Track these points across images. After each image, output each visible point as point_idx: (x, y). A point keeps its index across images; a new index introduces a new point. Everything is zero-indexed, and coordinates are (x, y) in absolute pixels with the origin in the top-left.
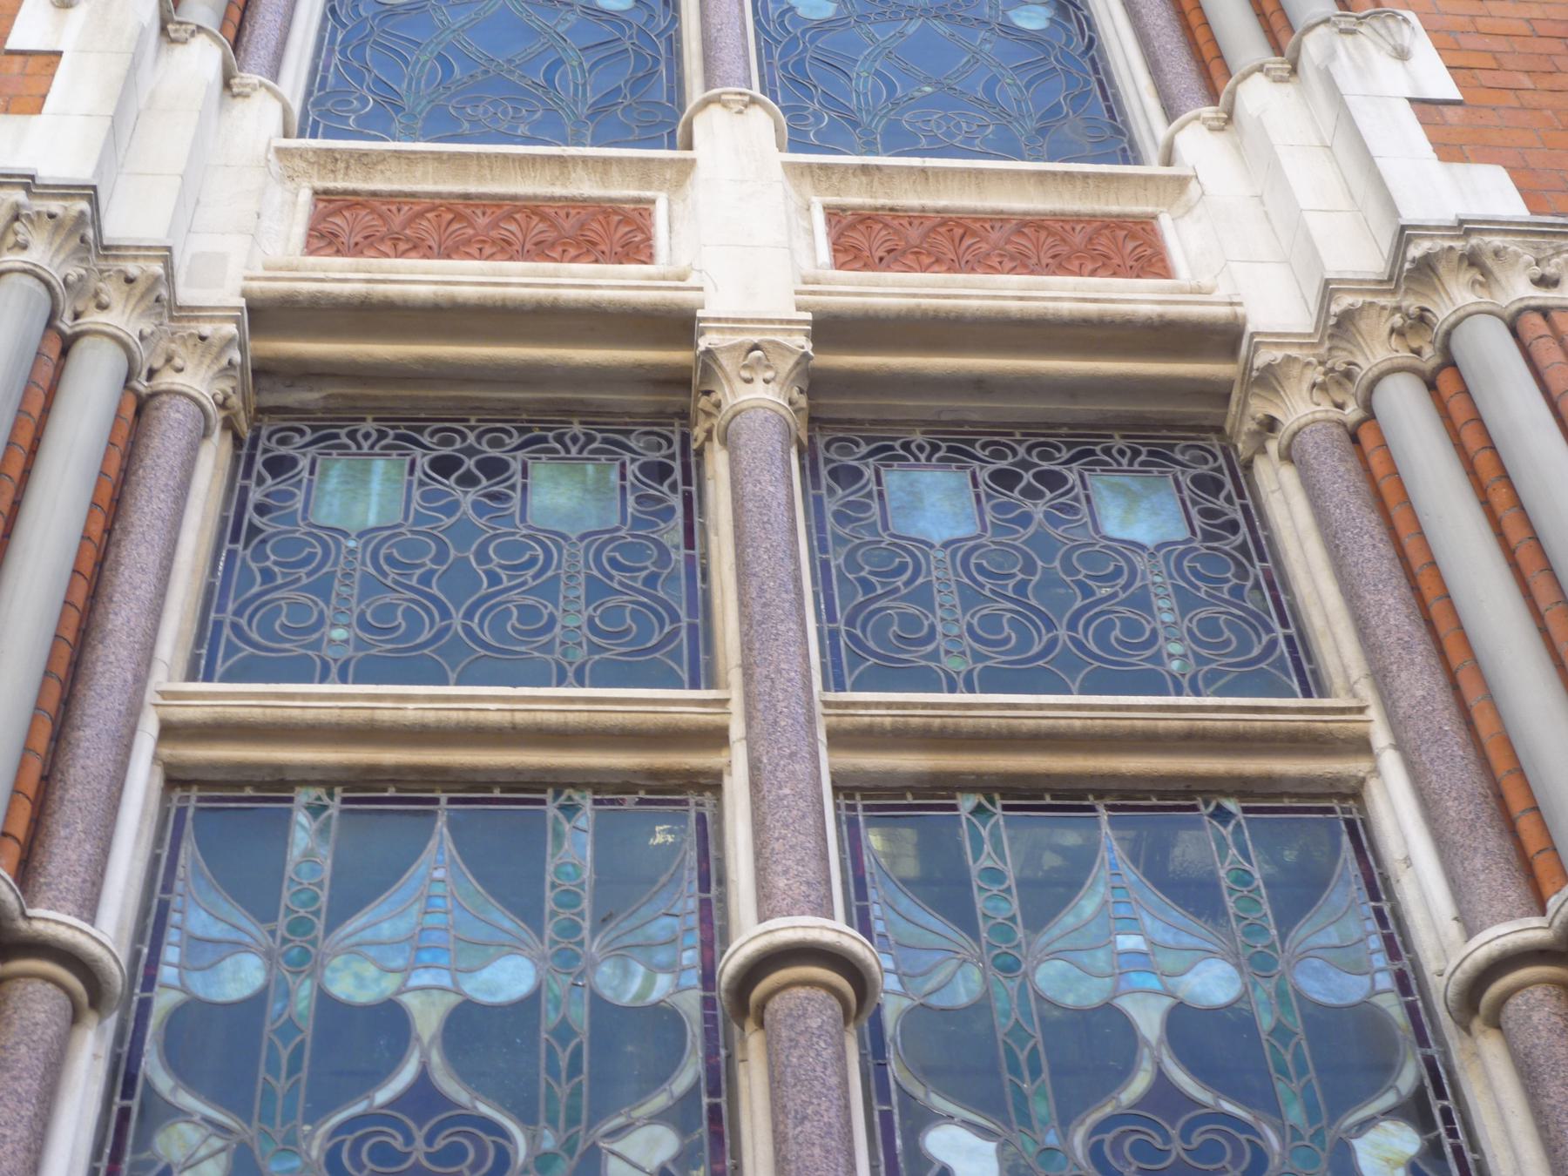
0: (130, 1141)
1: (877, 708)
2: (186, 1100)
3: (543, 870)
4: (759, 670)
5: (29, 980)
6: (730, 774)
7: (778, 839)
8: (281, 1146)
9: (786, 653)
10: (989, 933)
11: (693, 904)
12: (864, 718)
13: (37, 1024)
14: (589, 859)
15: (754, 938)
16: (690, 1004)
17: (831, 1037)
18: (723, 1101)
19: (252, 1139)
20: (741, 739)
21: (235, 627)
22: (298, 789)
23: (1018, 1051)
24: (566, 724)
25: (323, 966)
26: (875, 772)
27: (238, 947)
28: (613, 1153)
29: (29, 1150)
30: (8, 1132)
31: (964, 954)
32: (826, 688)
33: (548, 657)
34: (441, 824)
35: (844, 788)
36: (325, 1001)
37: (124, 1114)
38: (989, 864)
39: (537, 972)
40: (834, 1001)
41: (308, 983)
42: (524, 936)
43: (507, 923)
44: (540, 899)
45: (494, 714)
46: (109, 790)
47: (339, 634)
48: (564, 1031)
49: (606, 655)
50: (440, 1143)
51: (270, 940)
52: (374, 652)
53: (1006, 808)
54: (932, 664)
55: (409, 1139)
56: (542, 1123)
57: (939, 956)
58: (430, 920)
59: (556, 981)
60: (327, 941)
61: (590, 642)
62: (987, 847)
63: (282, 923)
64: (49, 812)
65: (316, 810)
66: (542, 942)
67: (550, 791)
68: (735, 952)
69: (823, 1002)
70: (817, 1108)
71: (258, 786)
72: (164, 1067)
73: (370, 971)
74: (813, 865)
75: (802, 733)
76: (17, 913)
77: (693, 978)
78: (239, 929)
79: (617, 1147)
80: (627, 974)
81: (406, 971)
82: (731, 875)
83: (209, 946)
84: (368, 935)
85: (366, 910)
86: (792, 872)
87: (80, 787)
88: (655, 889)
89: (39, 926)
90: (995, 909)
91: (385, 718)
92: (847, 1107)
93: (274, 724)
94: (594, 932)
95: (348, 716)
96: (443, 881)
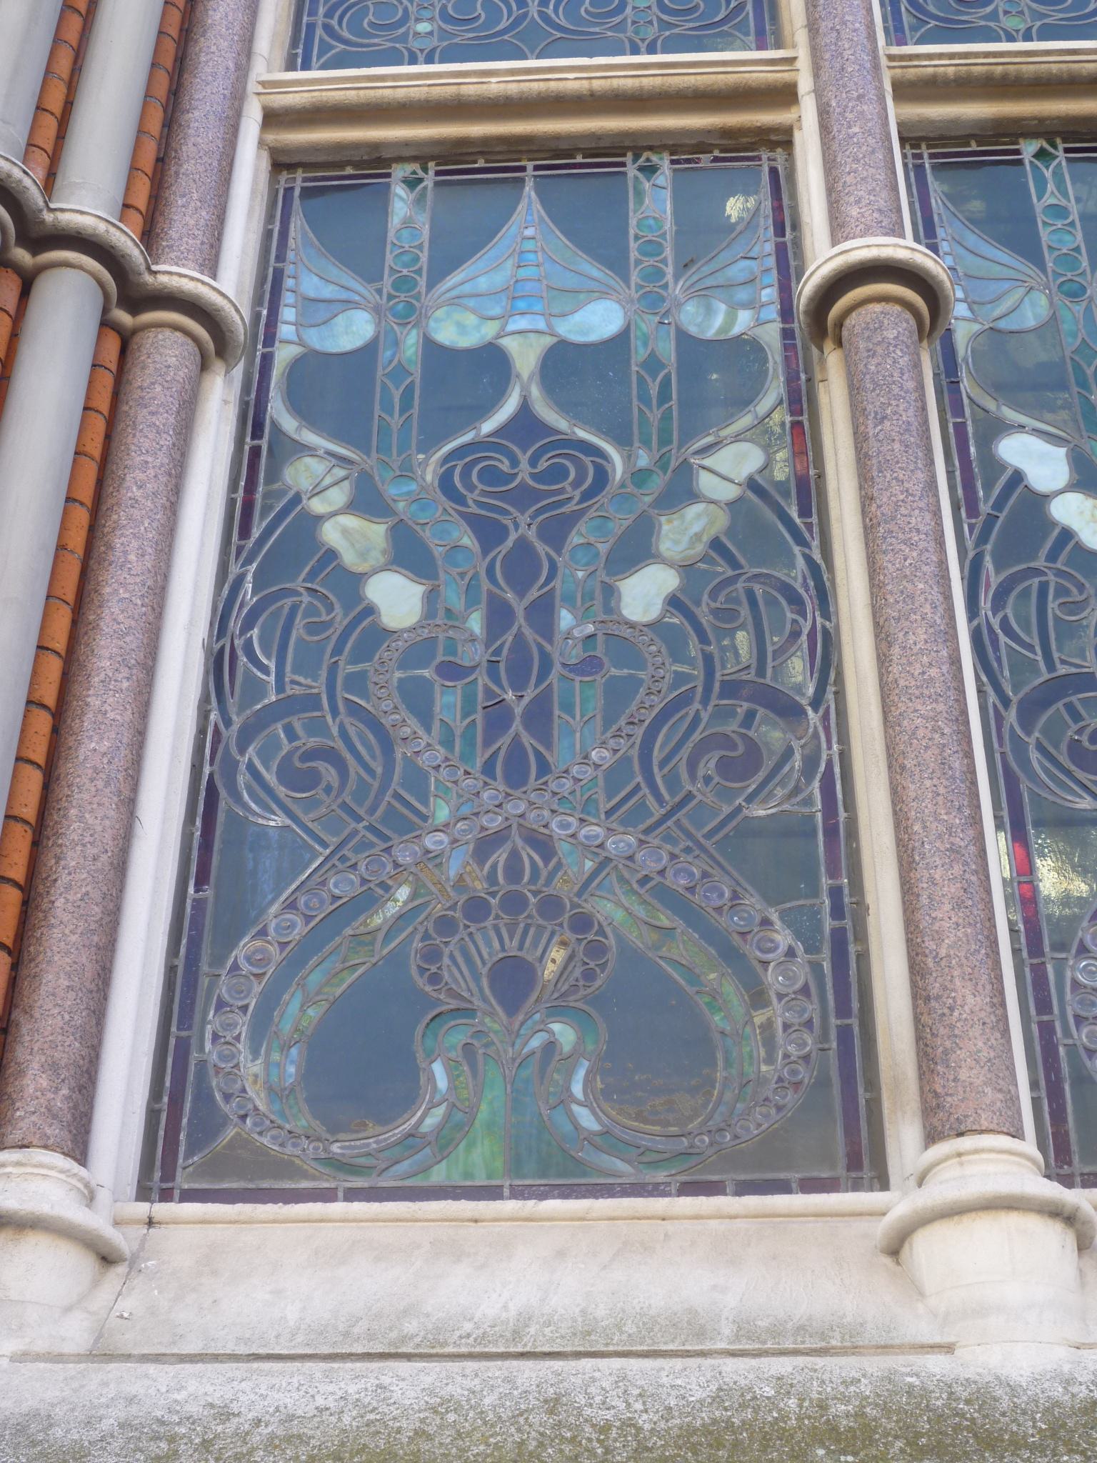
0: (262, 475)
1: (940, 59)
2: (310, 437)
3: (627, 224)
4: (824, 24)
5: (159, 330)
6: (800, 129)
7: (849, 173)
8: (398, 473)
9: (850, 6)
10: (1054, 263)
11: (769, 247)
12: (928, 69)
13: (169, 367)
14: (669, 212)
15: (831, 258)
16: (771, 335)
17: (907, 347)
18: (805, 418)
19: (372, 468)
20: (809, 93)
21: (327, 28)
22: (394, 165)
23: (1085, 367)
24: (641, 88)
25: (428, 318)
26: (940, 121)
27: (348, 304)
28: (704, 468)
29: (170, 475)
30: (150, 459)
31: (1033, 283)
32: (889, 43)
33: (621, 35)
34: (529, 188)
35: (911, 138)
36: (430, 346)
37: (255, 452)
38: (1053, 201)
39: (625, 313)
40: (908, 315)
41: (414, 332)
42: (612, 282)
43: (595, 273)
44: (626, 250)
45: (572, 84)
46: (219, 165)
47: (423, 27)
48: (653, 364)
49: (676, 31)
50: (543, 465)
51: (378, 297)
52: (457, 40)
53: (1067, 150)
54: (992, 24)
55: (515, 462)
56: (637, 444)
57: (1007, 285)
58: (522, 273)
59: (643, 320)
60: (430, 296)
61: (660, 20)
62: (1051, 187)
63: (387, 281)
64: (166, 185)
65: (412, 183)
66: (629, 288)
67: (630, 155)
68: (812, 274)
69: (898, 316)
70: (895, 409)
71: (356, 165)
72: (287, 410)
73: (471, 319)
74: (884, 194)
75: (869, 77)
76: (143, 267)
77: (772, 313)
78: (348, 289)
79: (707, 462)
80: (709, 311)
81: (504, 318)
82: (805, 218)
83: (322, 305)
84: (467, 288)
85: (465, 266)
86: (864, 202)
87: (193, 162)
88: (733, 235)
89: (163, 279)
90: (1060, 241)
91: (471, 93)
92: (924, 408)
93: (368, 105)
94: (677, 278)
95: (437, 92)
96: (533, 238)
